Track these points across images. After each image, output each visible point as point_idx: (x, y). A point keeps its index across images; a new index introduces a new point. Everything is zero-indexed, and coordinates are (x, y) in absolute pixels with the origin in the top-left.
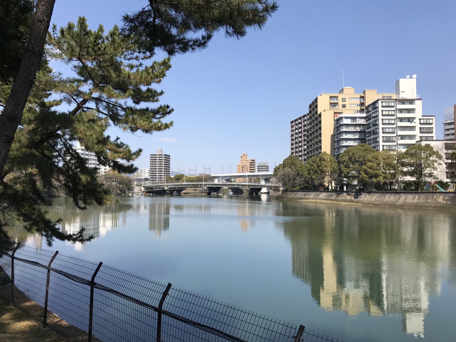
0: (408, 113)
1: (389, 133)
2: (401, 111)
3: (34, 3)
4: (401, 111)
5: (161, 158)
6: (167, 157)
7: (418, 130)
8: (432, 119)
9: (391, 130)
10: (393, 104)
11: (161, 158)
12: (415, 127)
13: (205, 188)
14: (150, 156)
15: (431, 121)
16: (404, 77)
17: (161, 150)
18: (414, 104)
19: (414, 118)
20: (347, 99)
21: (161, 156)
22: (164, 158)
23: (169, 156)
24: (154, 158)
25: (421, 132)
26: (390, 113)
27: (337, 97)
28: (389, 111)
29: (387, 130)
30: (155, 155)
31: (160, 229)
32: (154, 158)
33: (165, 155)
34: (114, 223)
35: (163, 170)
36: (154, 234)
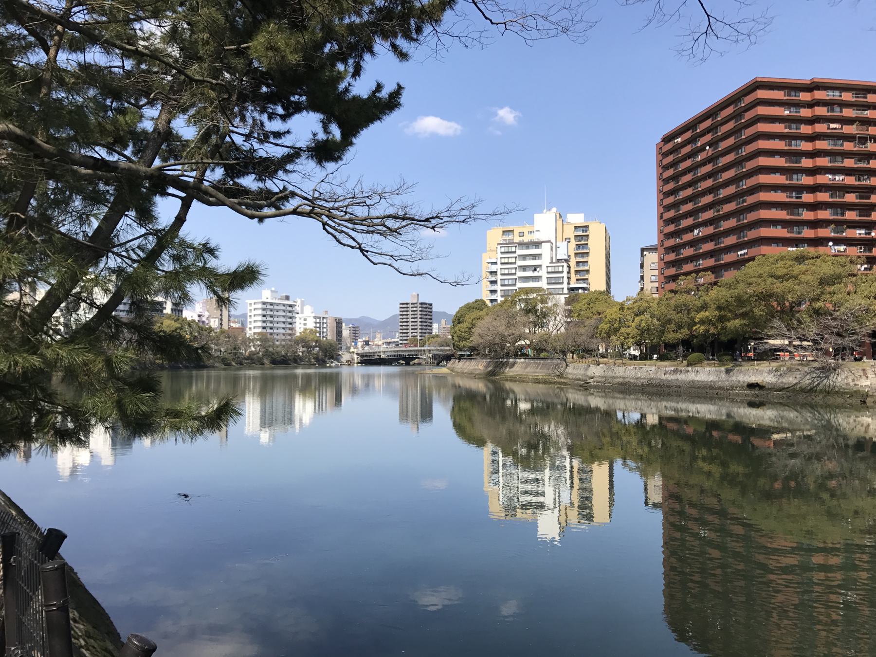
0: (533, 259)
1: (508, 285)
2: (524, 257)
3: (58, 212)
4: (524, 257)
5: (414, 309)
6: (425, 306)
7: (545, 280)
8: (563, 266)
9: (510, 282)
10: (513, 249)
11: (414, 309)
12: (541, 277)
13: (430, 355)
14: (399, 306)
15: (560, 269)
16: (540, 212)
17: (418, 295)
18: (541, 248)
19: (540, 266)
20: (526, 233)
21: (415, 305)
22: (419, 309)
23: (431, 305)
24: (405, 309)
25: (548, 284)
26: (510, 260)
27: (512, 231)
28: (508, 258)
29: (506, 282)
30: (407, 304)
31: (415, 421)
32: (405, 309)
33: (421, 303)
34: (317, 403)
35: (419, 327)
36: (408, 428)
